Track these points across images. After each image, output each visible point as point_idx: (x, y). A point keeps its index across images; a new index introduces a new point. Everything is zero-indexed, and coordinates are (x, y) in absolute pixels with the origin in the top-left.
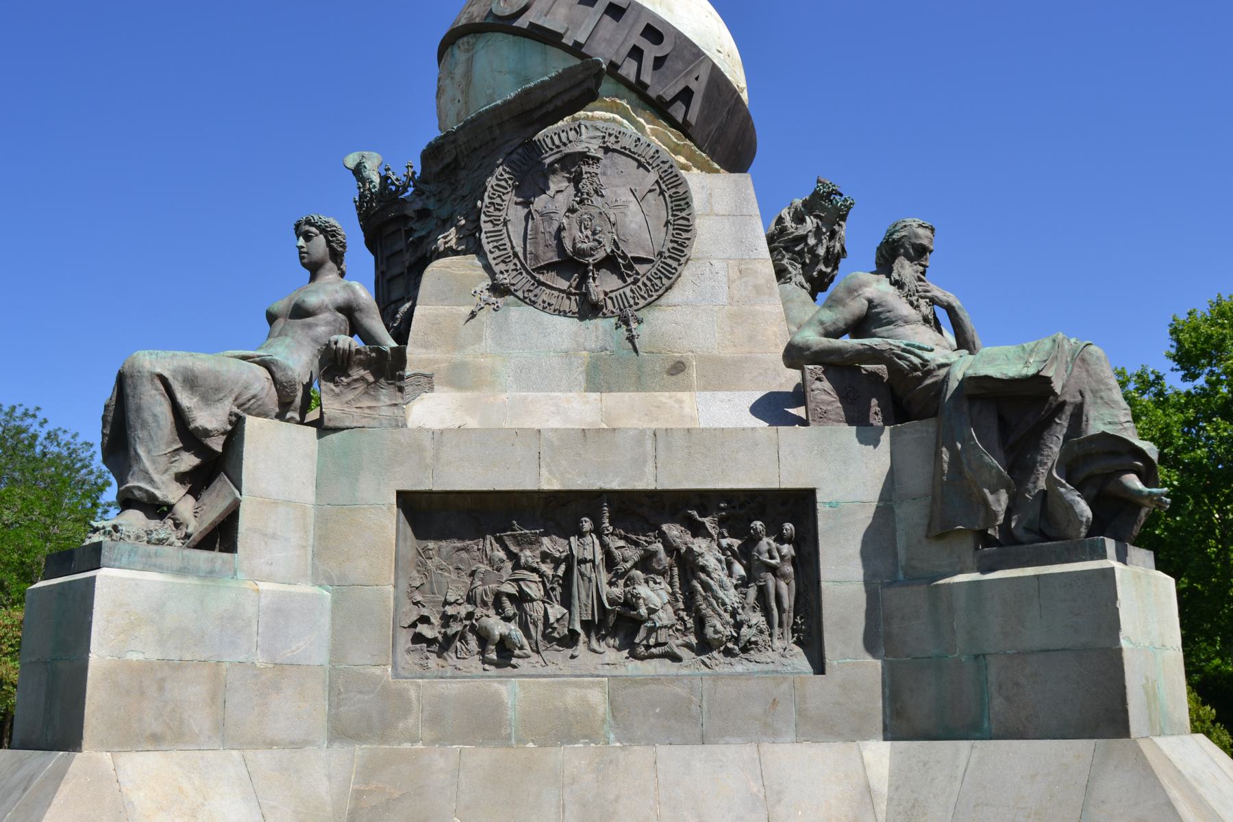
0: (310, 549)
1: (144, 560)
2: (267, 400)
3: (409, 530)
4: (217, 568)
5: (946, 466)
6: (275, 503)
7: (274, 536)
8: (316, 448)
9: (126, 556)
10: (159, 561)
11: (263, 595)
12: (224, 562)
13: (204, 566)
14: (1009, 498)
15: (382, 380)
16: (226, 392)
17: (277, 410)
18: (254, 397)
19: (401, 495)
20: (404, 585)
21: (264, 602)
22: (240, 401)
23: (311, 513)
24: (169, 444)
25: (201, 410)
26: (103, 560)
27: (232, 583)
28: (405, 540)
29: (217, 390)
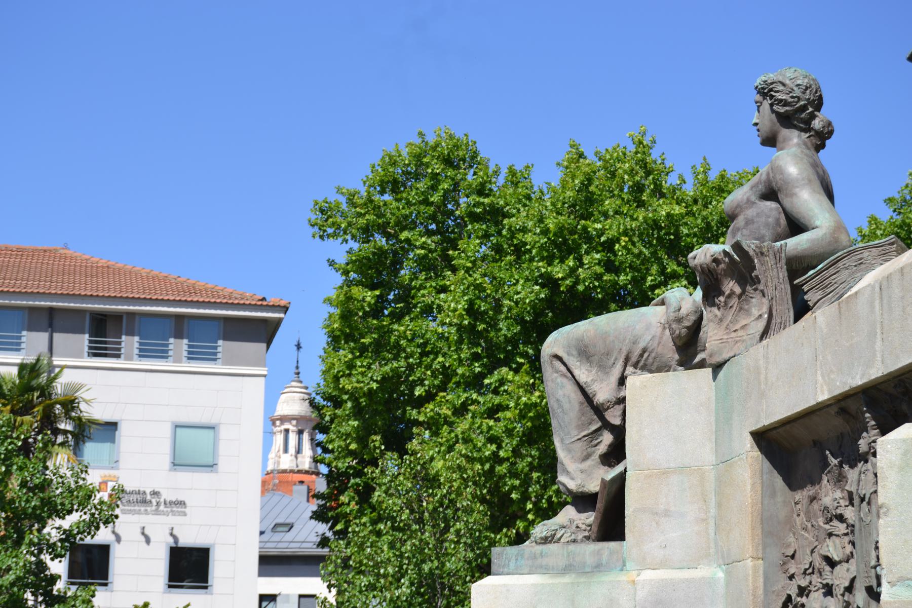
0: (712, 523)
1: (530, 562)
2: (660, 350)
3: (779, 481)
4: (604, 562)
5: (736, 257)
6: (666, 473)
7: (667, 513)
8: (713, 394)
9: (513, 561)
10: (544, 561)
11: (639, 587)
12: (611, 553)
13: (590, 561)
14: (542, 339)
15: (749, 288)
16: (615, 355)
17: (677, 357)
18: (644, 351)
19: (764, 438)
20: (776, 556)
21: (641, 594)
22: (634, 359)
23: (711, 476)
24: (581, 427)
25: (602, 381)
26: (494, 568)
27: (623, 577)
28: (773, 494)
29: (608, 354)
